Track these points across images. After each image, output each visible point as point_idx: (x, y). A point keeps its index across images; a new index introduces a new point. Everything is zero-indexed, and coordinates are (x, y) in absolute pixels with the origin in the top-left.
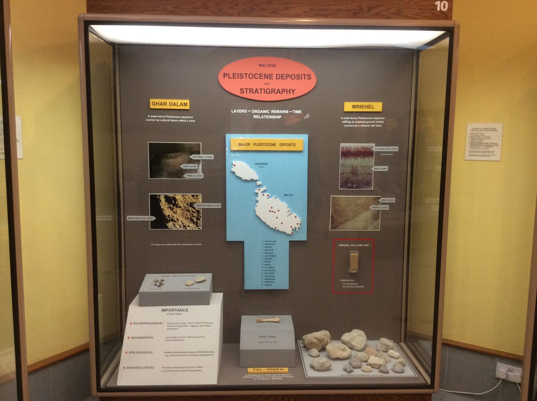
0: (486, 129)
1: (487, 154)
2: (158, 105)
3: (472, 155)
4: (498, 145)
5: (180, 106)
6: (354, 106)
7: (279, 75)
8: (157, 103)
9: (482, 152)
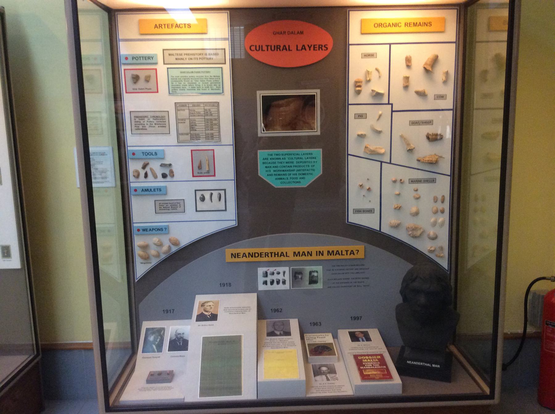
2: (276, 256)
5: (242, 257)
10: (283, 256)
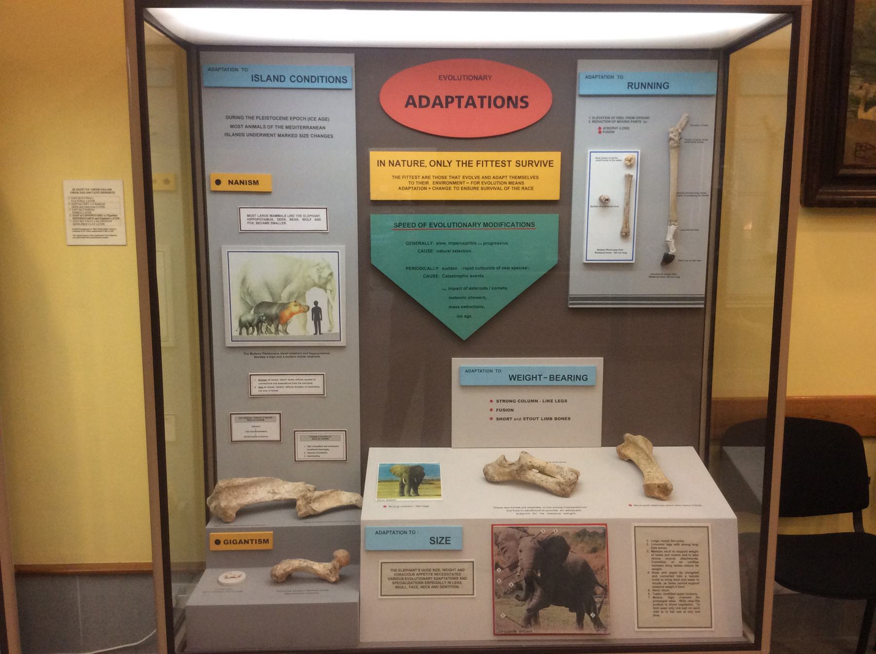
0: (96, 191)
1: (104, 233)
3: (79, 237)
4: (119, 218)
5: (267, 81)
6: (513, 379)
7: (315, 77)
8: (533, 377)
9: (95, 230)
10: (564, 380)
